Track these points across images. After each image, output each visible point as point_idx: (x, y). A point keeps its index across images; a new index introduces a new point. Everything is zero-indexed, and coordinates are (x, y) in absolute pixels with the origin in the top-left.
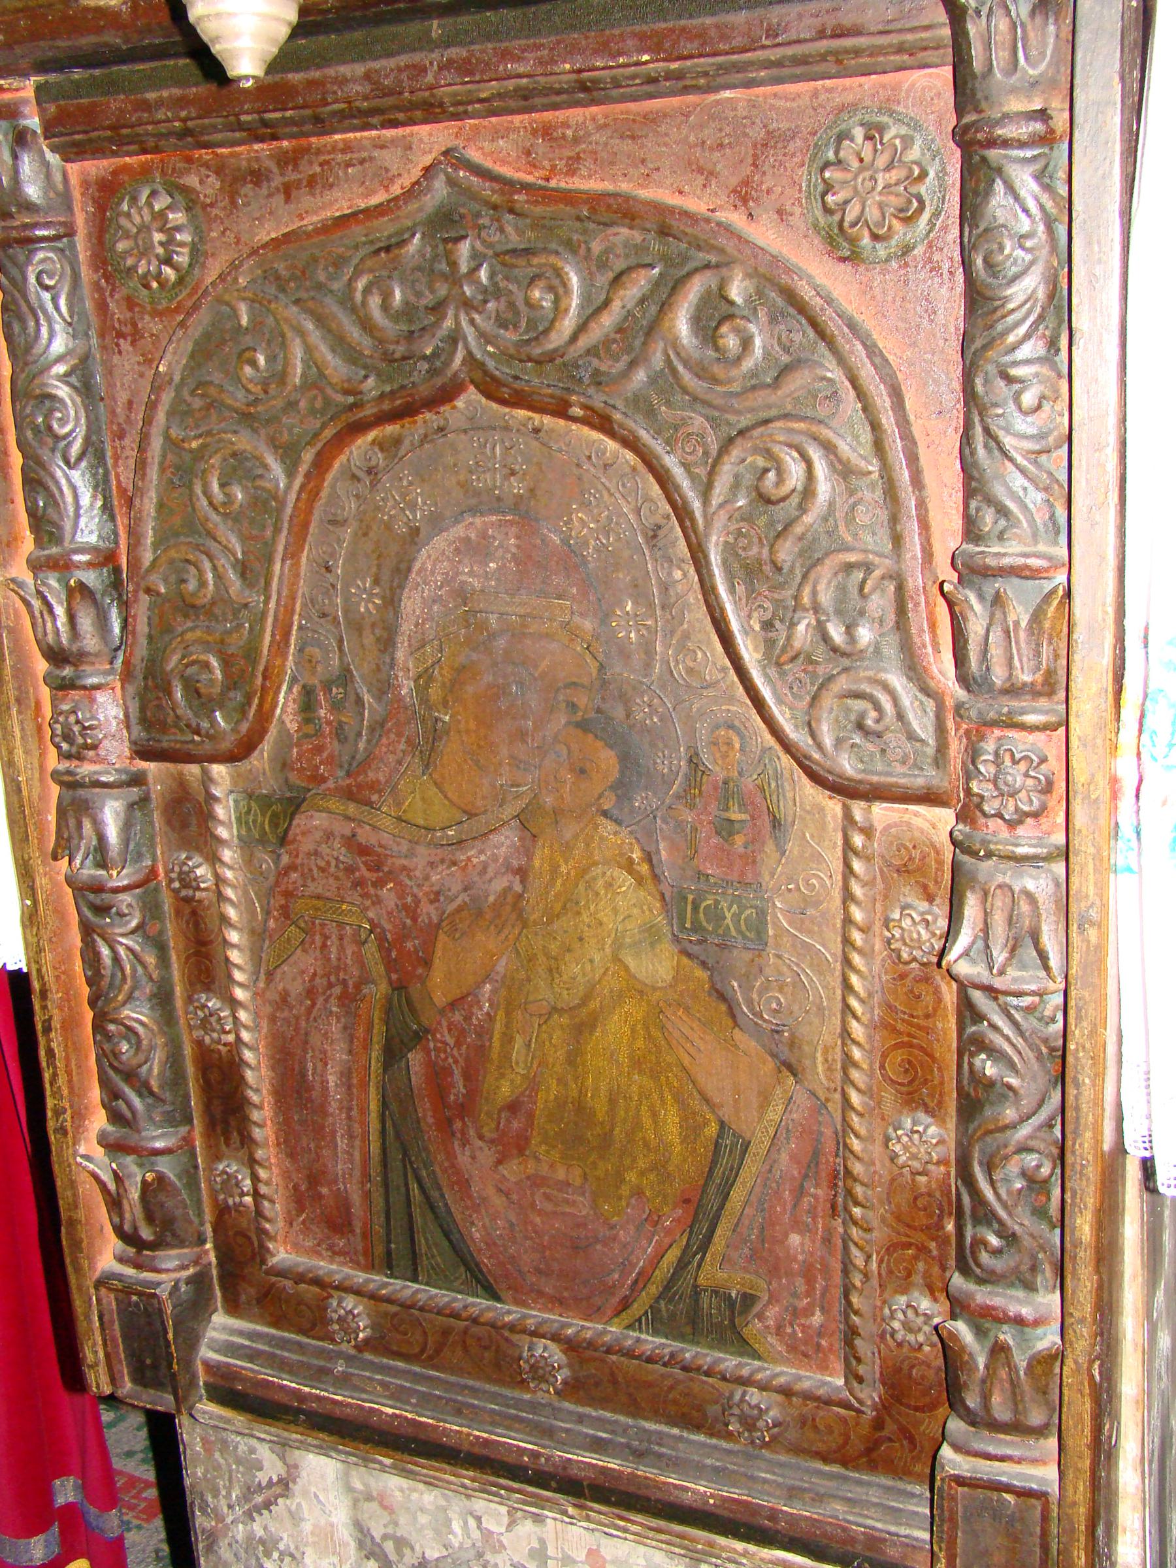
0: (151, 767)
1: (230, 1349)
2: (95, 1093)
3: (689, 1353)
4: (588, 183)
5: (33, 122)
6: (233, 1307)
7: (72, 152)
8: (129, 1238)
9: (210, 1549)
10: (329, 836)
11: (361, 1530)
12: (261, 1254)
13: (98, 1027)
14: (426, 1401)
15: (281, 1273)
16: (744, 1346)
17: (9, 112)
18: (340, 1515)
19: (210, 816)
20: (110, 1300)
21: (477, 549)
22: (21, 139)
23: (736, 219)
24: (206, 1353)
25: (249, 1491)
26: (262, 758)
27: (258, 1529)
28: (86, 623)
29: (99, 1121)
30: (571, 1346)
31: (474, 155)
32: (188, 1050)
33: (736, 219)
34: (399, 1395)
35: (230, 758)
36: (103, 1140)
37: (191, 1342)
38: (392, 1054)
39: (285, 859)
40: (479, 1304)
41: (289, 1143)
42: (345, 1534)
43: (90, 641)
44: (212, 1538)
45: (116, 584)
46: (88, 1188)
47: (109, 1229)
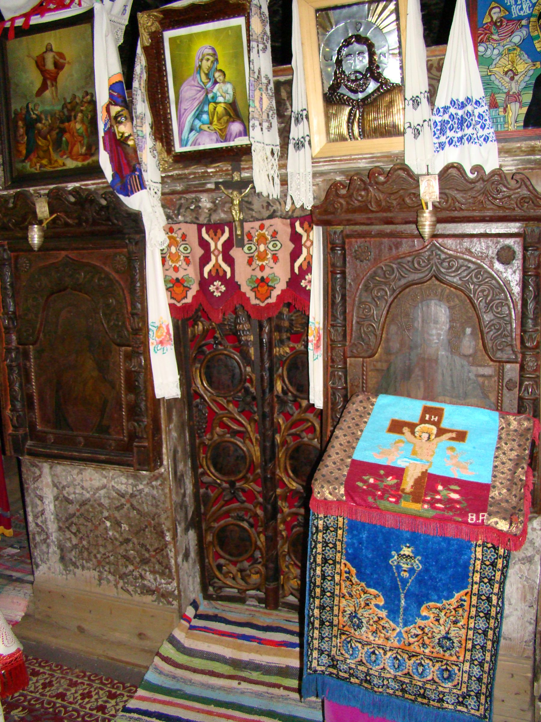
0: (20, 346)
1: (30, 446)
2: (9, 402)
3: (102, 436)
4: (85, 261)
5: (6, 247)
6: (31, 440)
7: (12, 251)
8: (14, 426)
9: (27, 491)
10: (534, 476)
11: (53, 481)
12: (36, 428)
13: (10, 390)
14: (61, 450)
15: (39, 431)
16: (109, 434)
17: (3, 246)
18: (49, 480)
19: (33, 398)
20: (11, 438)
21: (70, 312)
22: (5, 250)
23: (103, 267)
24: (26, 446)
25: (34, 478)
26: (38, 345)
27: (36, 485)
28: (11, 323)
29: (10, 407)
30: (84, 437)
31: (70, 256)
32: (25, 394)
33: (103, 267)
34: (58, 449)
35: (33, 344)
36: (10, 410)
37: (24, 445)
38: (57, 391)
39: (473, 678)
40: (70, 433)
41: (41, 409)
42: (50, 483)
43: (11, 326)
44: (28, 488)
45: (16, 317)
46: (8, 418)
47: (11, 426)
